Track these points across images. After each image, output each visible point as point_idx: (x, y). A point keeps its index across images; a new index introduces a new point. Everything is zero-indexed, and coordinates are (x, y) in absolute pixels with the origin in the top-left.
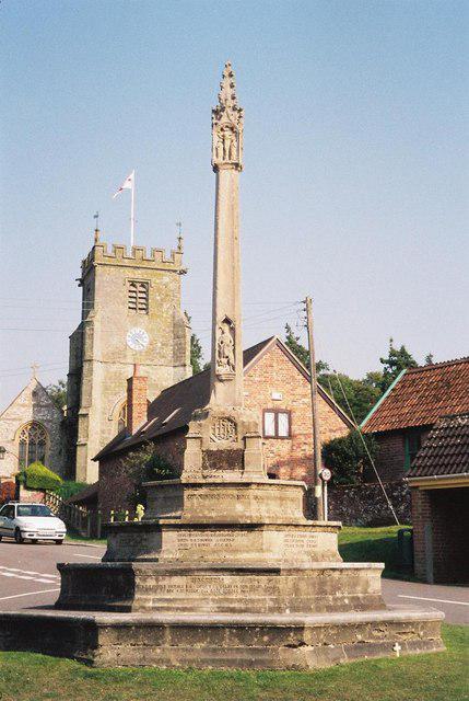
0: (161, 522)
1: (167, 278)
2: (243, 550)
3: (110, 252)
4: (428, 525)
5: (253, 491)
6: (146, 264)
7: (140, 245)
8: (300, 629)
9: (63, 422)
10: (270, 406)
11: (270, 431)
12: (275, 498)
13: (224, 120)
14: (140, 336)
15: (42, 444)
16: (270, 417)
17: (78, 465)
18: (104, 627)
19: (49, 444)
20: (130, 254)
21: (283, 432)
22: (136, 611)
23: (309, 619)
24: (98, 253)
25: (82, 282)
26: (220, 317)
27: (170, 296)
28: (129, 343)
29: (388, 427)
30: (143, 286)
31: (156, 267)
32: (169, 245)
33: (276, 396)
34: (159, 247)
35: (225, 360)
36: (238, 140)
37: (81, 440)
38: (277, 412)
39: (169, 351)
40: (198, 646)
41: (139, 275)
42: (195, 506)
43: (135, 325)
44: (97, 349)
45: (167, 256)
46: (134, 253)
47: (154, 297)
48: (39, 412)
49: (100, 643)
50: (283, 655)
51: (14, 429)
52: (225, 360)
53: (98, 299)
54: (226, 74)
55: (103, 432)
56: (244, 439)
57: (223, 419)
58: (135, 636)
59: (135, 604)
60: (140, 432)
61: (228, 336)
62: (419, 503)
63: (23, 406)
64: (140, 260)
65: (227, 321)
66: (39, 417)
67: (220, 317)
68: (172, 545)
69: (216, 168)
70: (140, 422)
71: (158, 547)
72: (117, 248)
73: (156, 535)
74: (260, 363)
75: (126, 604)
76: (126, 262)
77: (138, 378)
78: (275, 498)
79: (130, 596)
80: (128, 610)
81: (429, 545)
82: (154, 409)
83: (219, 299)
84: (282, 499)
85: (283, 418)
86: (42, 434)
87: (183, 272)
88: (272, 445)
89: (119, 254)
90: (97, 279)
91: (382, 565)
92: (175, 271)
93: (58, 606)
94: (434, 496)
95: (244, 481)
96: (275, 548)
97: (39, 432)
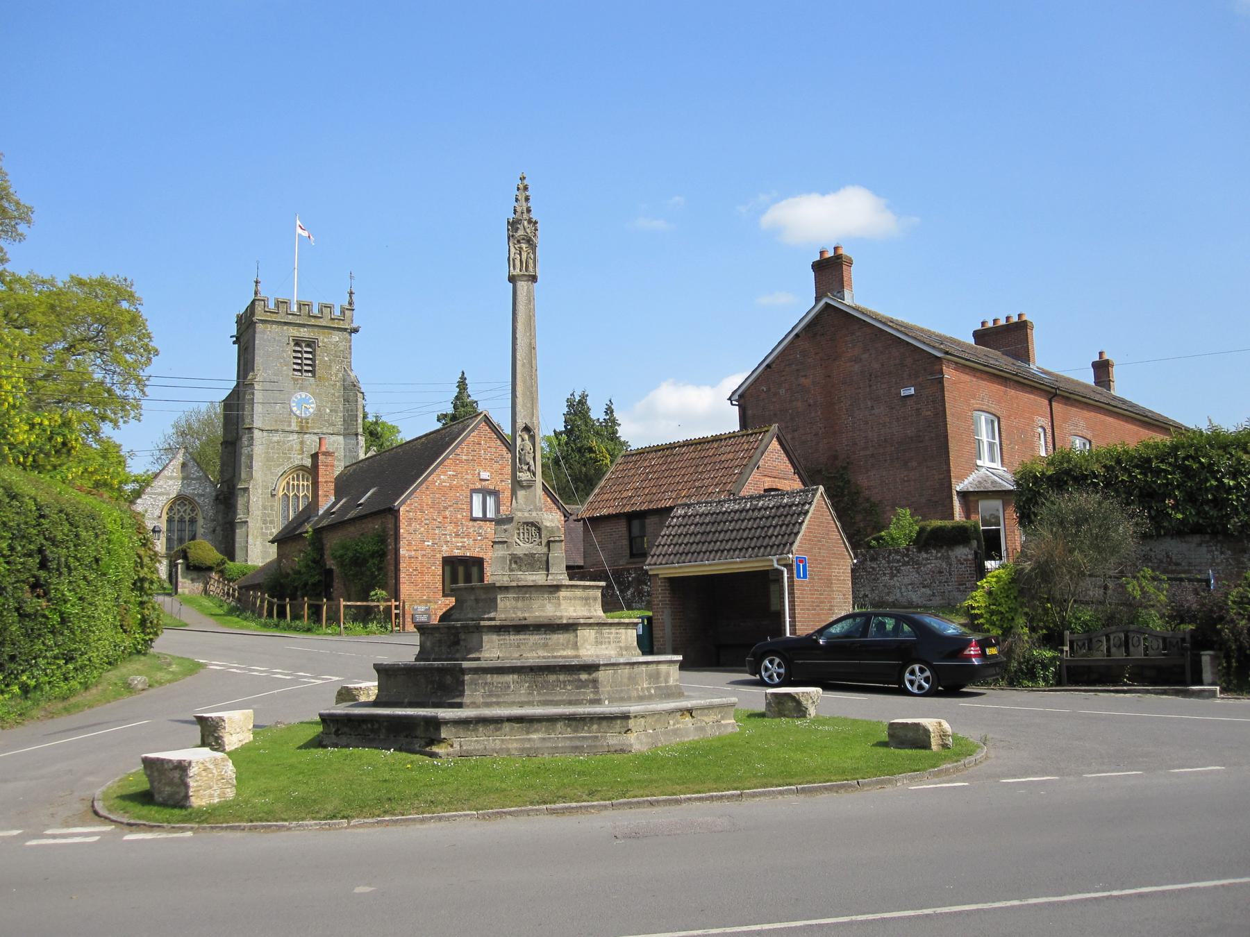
0: (482, 623)
1: (336, 337)
2: (559, 650)
3: (272, 306)
4: (667, 612)
5: (563, 594)
6: (313, 321)
7: (305, 299)
8: (625, 717)
9: (217, 498)
10: (478, 486)
11: (477, 513)
12: (581, 598)
13: (521, 232)
14: (306, 401)
15: (193, 521)
16: (477, 499)
17: (237, 545)
18: (446, 722)
19: (201, 522)
20: (295, 309)
21: (490, 514)
22: (468, 707)
23: (634, 708)
24: (259, 308)
25: (238, 340)
26: (520, 424)
27: (344, 356)
28: (294, 409)
29: (612, 511)
30: (308, 346)
31: (324, 324)
32: (341, 301)
33: (485, 475)
34: (328, 302)
35: (525, 467)
36: (534, 253)
37: (240, 516)
38: (486, 492)
39: (339, 420)
40: (534, 736)
41: (304, 333)
42: (507, 609)
43: (301, 389)
44: (259, 416)
45: (337, 312)
46: (300, 309)
47: (323, 357)
48: (189, 485)
49: (443, 736)
50: (613, 738)
51: (161, 505)
52: (525, 467)
53: (259, 360)
54: (521, 186)
55: (265, 508)
56: (549, 543)
57: (527, 524)
58: (475, 730)
59: (466, 700)
60: (328, 513)
61: (528, 444)
62: (660, 594)
63: (171, 478)
64: (307, 316)
65: (527, 429)
66: (188, 491)
67: (520, 424)
68: (493, 650)
69: (512, 279)
70: (327, 501)
71: (479, 648)
72: (278, 303)
73: (476, 635)
74: (470, 439)
75: (458, 700)
76: (290, 319)
77: (327, 454)
78: (581, 598)
79: (462, 694)
80: (460, 705)
81: (668, 630)
82: (343, 486)
83: (519, 407)
84: (587, 599)
85: (490, 501)
86: (193, 510)
87: (356, 331)
88: (480, 527)
89: (282, 309)
90: (257, 336)
91: (680, 658)
92: (345, 330)
93: (375, 704)
94: (676, 584)
95: (549, 583)
96: (589, 647)
97: (188, 508)
